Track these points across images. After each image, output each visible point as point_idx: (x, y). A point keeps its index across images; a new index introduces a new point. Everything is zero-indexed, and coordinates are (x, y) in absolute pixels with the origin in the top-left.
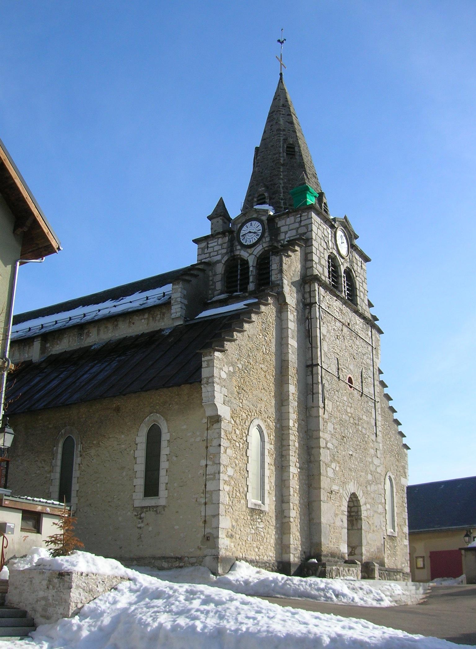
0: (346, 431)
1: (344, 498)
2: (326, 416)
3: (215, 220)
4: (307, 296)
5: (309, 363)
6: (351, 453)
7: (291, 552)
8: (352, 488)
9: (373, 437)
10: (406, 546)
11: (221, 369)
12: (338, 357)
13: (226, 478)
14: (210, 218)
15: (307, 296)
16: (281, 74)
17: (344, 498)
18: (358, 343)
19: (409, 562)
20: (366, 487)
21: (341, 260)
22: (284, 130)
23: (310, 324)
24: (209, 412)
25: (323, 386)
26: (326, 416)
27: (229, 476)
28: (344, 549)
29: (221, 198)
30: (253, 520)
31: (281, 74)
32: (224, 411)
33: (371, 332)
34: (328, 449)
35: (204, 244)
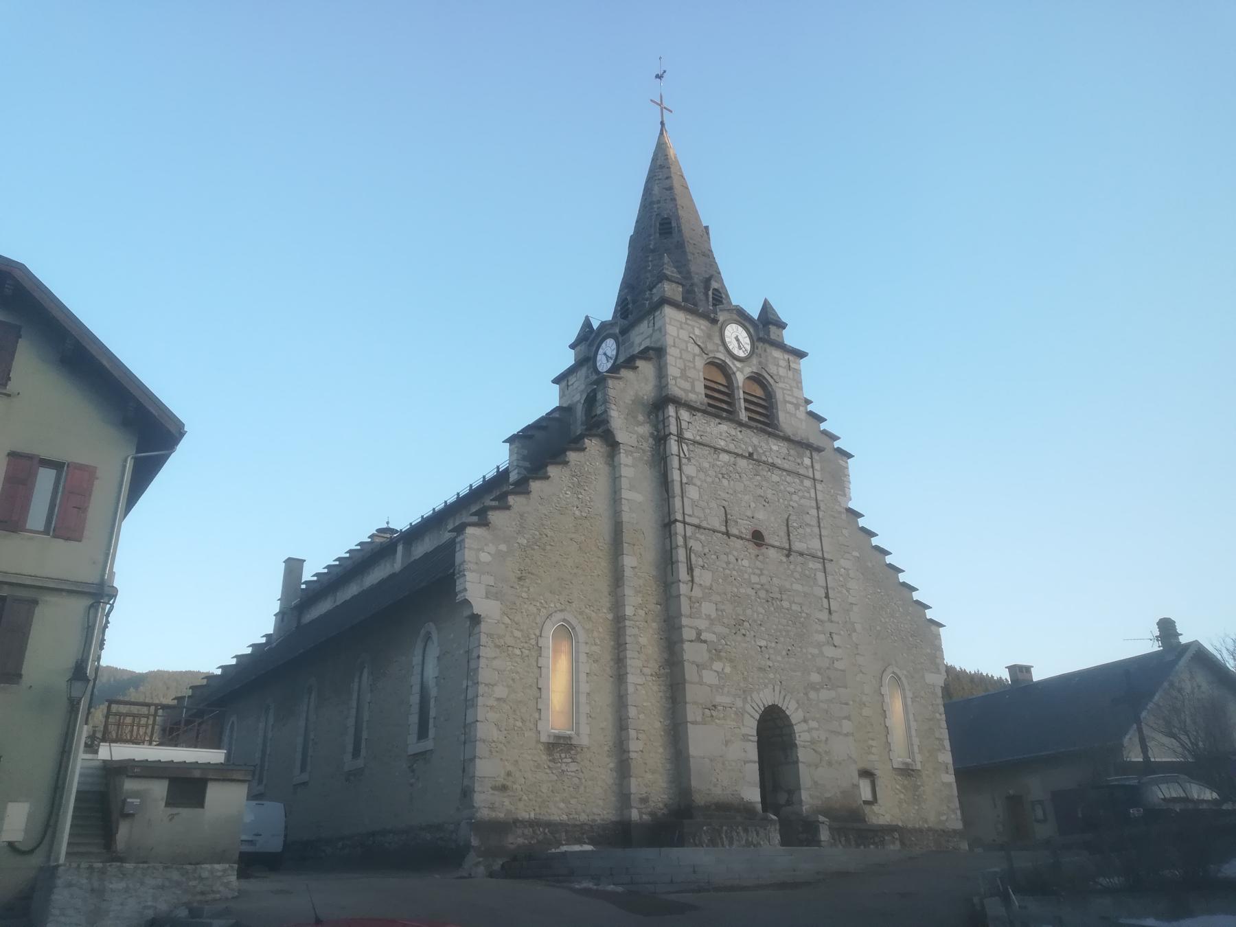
0: (749, 612)
1: (747, 716)
2: (697, 592)
3: (578, 348)
4: (661, 426)
5: (667, 521)
6: (763, 643)
7: (633, 804)
8: (767, 697)
9: (824, 616)
10: (949, 785)
11: (482, 550)
12: (725, 504)
13: (492, 702)
14: (572, 346)
15: (661, 426)
16: (662, 123)
17: (747, 716)
18: (775, 478)
19: (959, 812)
20: (806, 694)
21: (734, 366)
22: (659, 202)
23: (666, 463)
24: (467, 613)
25: (689, 551)
26: (697, 592)
27: (498, 699)
28: (753, 795)
29: (587, 318)
30: (553, 761)
31: (662, 123)
32: (481, 604)
33: (811, 458)
34: (705, 642)
35: (564, 383)
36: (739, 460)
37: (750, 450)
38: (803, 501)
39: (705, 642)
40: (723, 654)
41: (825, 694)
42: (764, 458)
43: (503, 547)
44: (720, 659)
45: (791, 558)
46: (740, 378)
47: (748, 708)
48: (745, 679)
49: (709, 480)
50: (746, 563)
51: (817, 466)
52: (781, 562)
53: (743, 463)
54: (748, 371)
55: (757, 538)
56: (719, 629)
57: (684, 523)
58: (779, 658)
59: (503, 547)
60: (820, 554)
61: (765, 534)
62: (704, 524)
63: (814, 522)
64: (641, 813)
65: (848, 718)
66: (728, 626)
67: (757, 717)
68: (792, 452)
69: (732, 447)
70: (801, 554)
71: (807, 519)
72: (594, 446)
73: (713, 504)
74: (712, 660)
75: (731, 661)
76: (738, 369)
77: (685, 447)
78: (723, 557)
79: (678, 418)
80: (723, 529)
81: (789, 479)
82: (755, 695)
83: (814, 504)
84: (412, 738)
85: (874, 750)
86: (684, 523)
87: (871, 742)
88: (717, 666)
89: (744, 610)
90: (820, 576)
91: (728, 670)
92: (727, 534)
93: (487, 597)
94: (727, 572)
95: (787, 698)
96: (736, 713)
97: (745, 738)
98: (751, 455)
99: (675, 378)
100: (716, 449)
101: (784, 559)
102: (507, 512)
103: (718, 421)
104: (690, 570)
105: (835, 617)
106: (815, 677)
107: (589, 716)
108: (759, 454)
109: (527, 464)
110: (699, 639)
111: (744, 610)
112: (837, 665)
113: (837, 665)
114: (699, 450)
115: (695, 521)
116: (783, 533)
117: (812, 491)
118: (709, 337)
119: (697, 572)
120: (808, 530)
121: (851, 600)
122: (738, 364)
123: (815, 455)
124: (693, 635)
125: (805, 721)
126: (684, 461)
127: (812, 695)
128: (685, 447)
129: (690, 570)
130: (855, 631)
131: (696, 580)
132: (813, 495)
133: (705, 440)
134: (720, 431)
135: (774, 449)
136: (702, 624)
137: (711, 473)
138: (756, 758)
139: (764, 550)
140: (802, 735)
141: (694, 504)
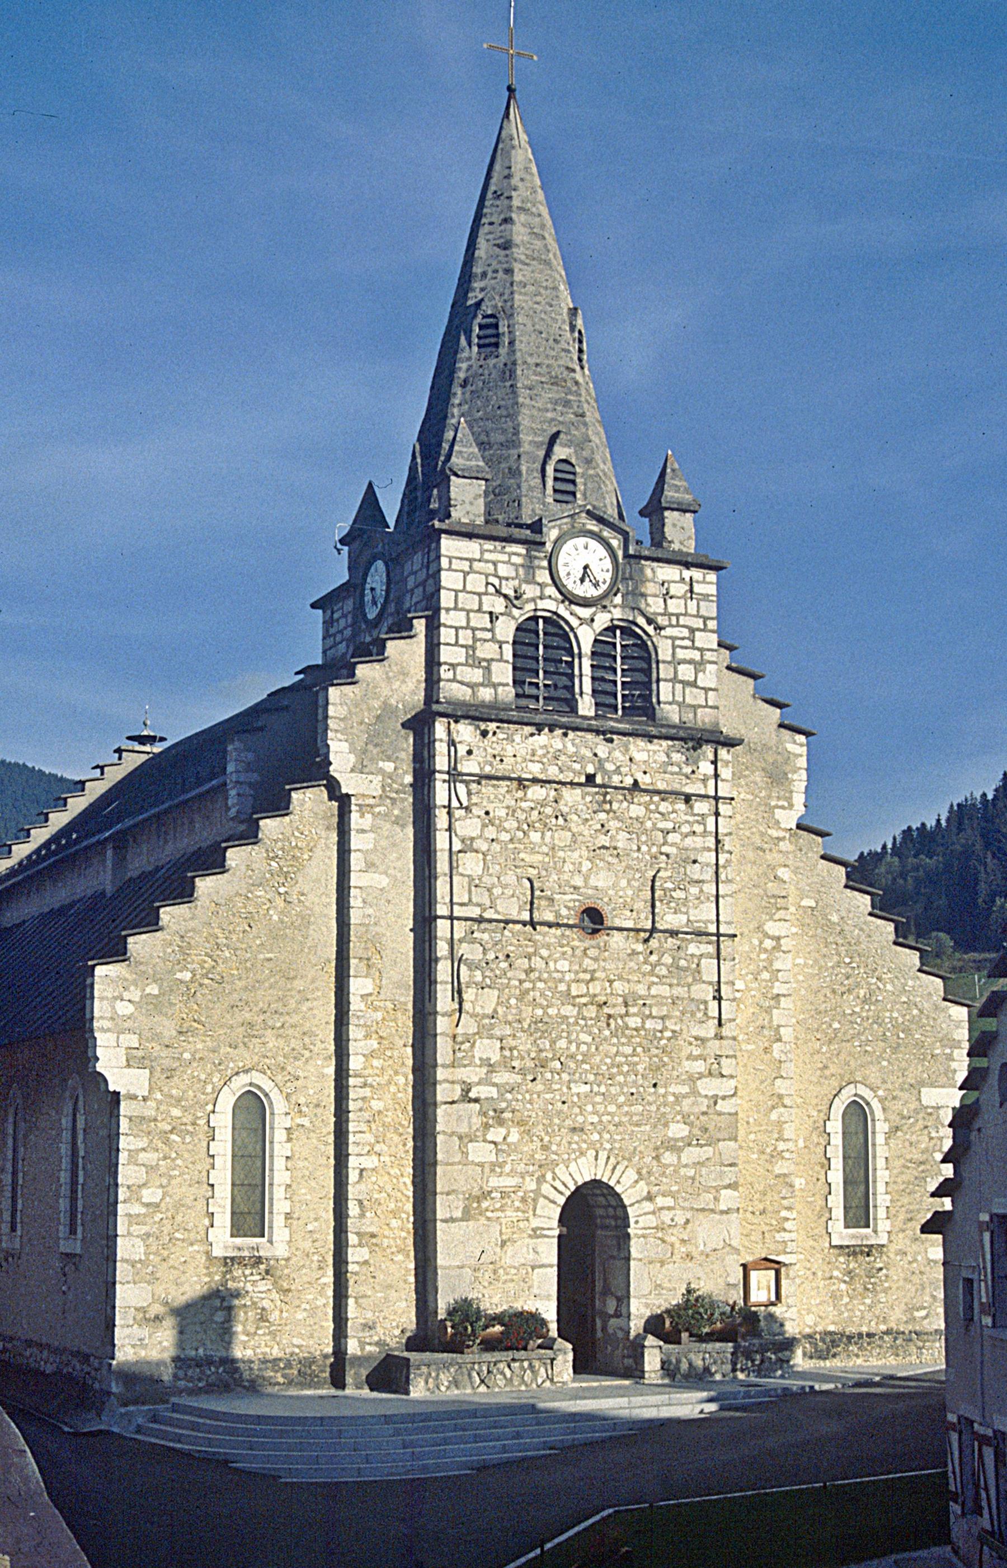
2: (468, 1026)
8: (584, 1171)
18: (636, 810)
20: (657, 1158)
33: (715, 762)
36: (566, 792)
37: (590, 769)
38: (689, 841)
39: (476, 1100)
40: (507, 1115)
41: (691, 1154)
42: (616, 780)
43: (153, 989)
44: (501, 1122)
45: (654, 943)
46: (586, 638)
47: (546, 1189)
48: (545, 1148)
49: (505, 837)
50: (563, 965)
51: (725, 773)
52: (634, 953)
53: (571, 796)
54: (602, 620)
55: (593, 920)
56: (503, 1077)
57: (451, 918)
58: (612, 1108)
59: (153, 989)
60: (712, 929)
61: (606, 910)
62: (489, 914)
63: (709, 874)
64: (362, 1344)
65: (733, 1186)
66: (522, 1071)
67: (562, 1200)
68: (676, 757)
69: (553, 772)
70: (673, 933)
71: (694, 871)
72: (308, 801)
73: (510, 878)
74: (487, 1126)
75: (520, 1123)
76: (582, 621)
77: (461, 788)
78: (524, 963)
79: (452, 743)
80: (526, 916)
81: (664, 807)
82: (561, 1171)
83: (711, 842)
84: (63, 1230)
85: (788, 1225)
86: (451, 918)
87: (784, 1213)
88: (496, 1134)
89: (553, 1042)
90: (709, 966)
91: (514, 1137)
92: (532, 923)
93: (129, 1066)
94: (527, 985)
95: (620, 1168)
96: (523, 1200)
97: (536, 1233)
98: (590, 779)
99: (453, 666)
100: (520, 780)
101: (640, 947)
102: (158, 934)
103: (528, 729)
104: (458, 992)
105: (725, 1031)
106: (678, 1130)
107: (288, 1216)
108: (605, 772)
109: (255, 777)
110: (466, 1097)
111: (553, 1042)
112: (721, 1106)
113: (721, 1106)
114: (487, 789)
115: (474, 912)
116: (642, 905)
117: (711, 820)
118: (530, 568)
119: (469, 995)
120: (694, 890)
121: (778, 988)
122: (585, 613)
123: (723, 753)
124: (457, 1092)
125: (650, 1198)
126: (458, 813)
127: (668, 1158)
128: (461, 788)
129: (458, 992)
130: (779, 1040)
131: (467, 1006)
132: (711, 827)
133: (500, 769)
134: (525, 749)
135: (645, 758)
136: (472, 1074)
137: (511, 824)
138: (555, 1261)
139: (602, 938)
140: (640, 1220)
141: (473, 883)
